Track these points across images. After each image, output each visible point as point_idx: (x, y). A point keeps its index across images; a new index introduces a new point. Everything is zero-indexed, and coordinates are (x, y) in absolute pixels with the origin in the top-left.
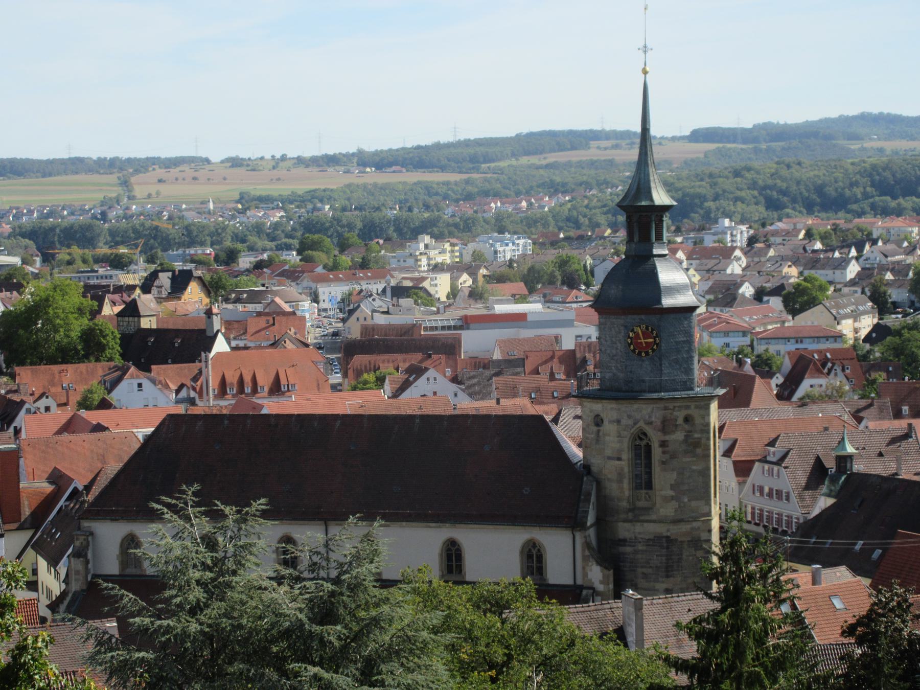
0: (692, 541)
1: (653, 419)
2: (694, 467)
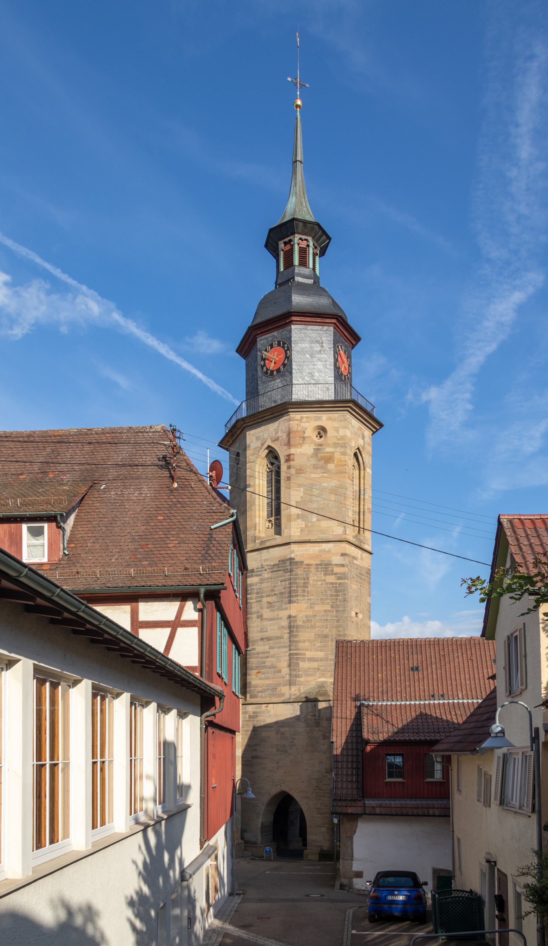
0: (321, 565)
1: (280, 434)
2: (325, 484)
